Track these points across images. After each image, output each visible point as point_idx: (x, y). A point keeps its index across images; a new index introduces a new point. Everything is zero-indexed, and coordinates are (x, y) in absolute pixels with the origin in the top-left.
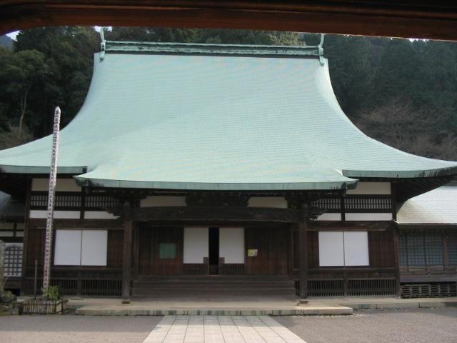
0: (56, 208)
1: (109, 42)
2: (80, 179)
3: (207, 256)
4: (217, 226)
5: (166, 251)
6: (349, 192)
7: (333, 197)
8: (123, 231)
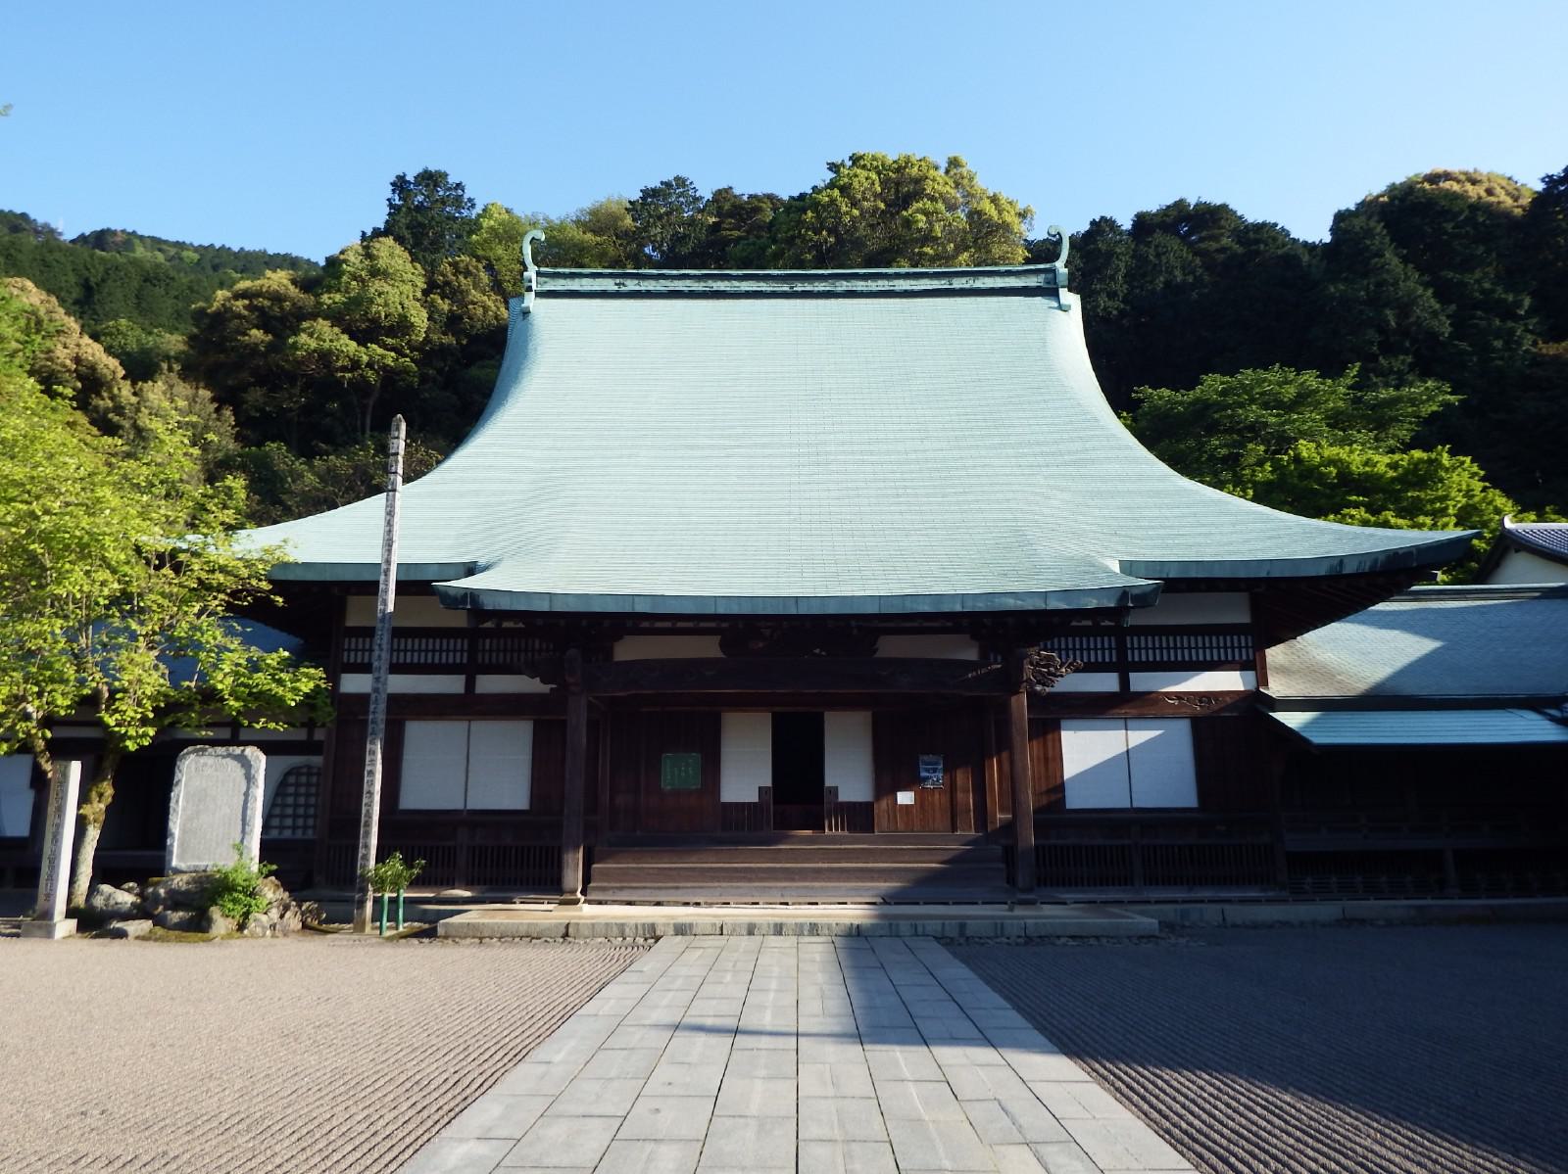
0: (396, 668)
1: (543, 269)
2: (452, 593)
3: (768, 782)
4: (384, 696)
5: (677, 772)
6: (1132, 620)
7: (1096, 631)
8: (564, 723)
